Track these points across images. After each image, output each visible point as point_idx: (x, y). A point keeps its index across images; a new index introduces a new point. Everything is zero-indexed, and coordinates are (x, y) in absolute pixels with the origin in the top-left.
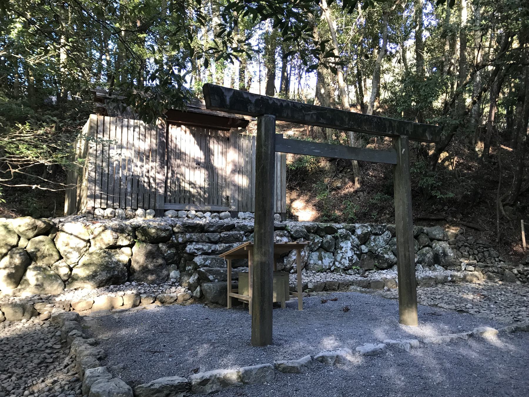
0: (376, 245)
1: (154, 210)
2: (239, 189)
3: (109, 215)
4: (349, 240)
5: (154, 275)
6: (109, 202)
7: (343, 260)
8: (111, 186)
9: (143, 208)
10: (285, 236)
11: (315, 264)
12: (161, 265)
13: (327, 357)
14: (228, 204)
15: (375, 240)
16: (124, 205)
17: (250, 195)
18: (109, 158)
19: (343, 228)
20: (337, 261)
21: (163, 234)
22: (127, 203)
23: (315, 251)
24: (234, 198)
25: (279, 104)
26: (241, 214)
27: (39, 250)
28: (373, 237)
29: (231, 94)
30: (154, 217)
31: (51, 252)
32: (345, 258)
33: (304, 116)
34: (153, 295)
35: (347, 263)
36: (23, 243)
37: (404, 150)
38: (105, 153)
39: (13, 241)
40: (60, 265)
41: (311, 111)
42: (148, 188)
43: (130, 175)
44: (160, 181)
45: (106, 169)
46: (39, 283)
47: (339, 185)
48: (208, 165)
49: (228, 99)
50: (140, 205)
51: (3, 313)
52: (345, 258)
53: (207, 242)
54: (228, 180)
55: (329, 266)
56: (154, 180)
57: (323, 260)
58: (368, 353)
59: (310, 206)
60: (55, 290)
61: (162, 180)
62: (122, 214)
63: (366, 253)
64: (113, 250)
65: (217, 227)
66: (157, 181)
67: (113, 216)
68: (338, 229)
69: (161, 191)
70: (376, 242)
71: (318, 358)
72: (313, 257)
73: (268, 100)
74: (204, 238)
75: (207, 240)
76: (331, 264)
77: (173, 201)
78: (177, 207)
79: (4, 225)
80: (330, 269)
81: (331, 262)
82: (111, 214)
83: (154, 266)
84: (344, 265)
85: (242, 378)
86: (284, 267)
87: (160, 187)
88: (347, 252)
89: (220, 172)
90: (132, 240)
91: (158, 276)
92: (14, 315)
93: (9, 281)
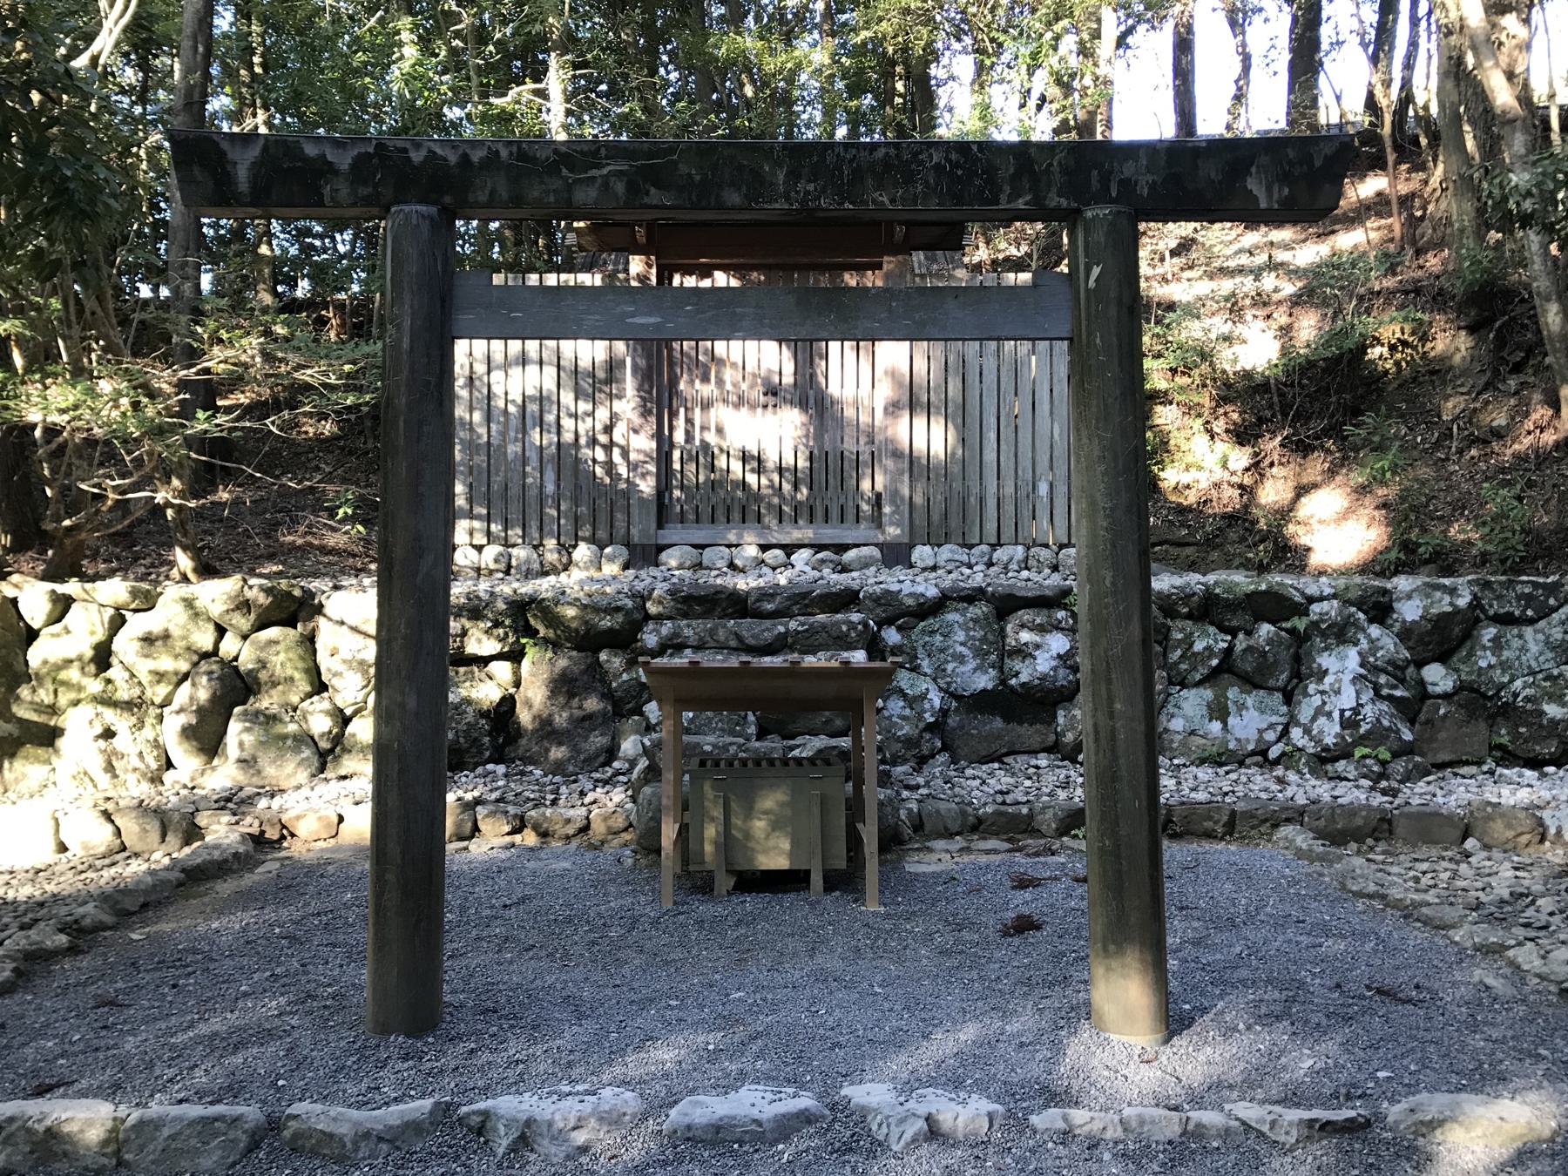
0: (1505, 666)
1: (627, 545)
2: (915, 466)
3: (492, 566)
4: (1356, 644)
5: (563, 748)
6: (493, 527)
7: (1322, 720)
8: (497, 480)
9: (592, 540)
10: (1057, 628)
11: (1193, 733)
12: (589, 717)
13: (499, 1118)
14: (877, 521)
15: (1498, 644)
16: (537, 535)
17: (957, 485)
18: (489, 396)
19: (1334, 596)
20: (1298, 724)
21: (606, 623)
22: (546, 529)
23: (1199, 684)
24: (895, 495)
25: (453, 158)
26: (922, 554)
27: (264, 667)
28: (1489, 633)
29: (254, 152)
30: (626, 567)
31: (289, 672)
32: (1329, 715)
33: (569, 188)
34: (512, 809)
35: (1330, 731)
36: (230, 645)
37: (1096, 271)
38: (477, 383)
39: (205, 640)
40: (311, 709)
41: (599, 166)
42: (607, 480)
43: (550, 444)
44: (641, 457)
45: (482, 431)
46: (245, 755)
47: (1501, 420)
48: (808, 395)
49: (242, 174)
50: (585, 531)
51: (118, 832)
52: (1329, 715)
53: (735, 649)
54: (879, 438)
55: (1260, 740)
56: (625, 453)
57: (1231, 721)
58: (689, 1127)
59: (1368, 510)
60: (289, 776)
61: (647, 455)
62: (528, 561)
63: (1446, 696)
64: (462, 670)
65: (788, 598)
66: (633, 456)
67: (502, 566)
68: (1311, 600)
69: (647, 486)
70: (1506, 654)
71: (468, 1115)
72: (1184, 705)
73: (405, 150)
74: (721, 635)
75: (733, 643)
76: (1270, 736)
77: (692, 517)
78: (700, 536)
79: (185, 600)
80: (1264, 753)
81: (1271, 726)
82: (496, 561)
83: (571, 719)
84: (1318, 742)
85: (116, 1140)
86: (1052, 738)
87: (643, 476)
88: (1338, 692)
89: (849, 413)
90: (511, 639)
91: (576, 750)
92: (141, 839)
93: (186, 746)
